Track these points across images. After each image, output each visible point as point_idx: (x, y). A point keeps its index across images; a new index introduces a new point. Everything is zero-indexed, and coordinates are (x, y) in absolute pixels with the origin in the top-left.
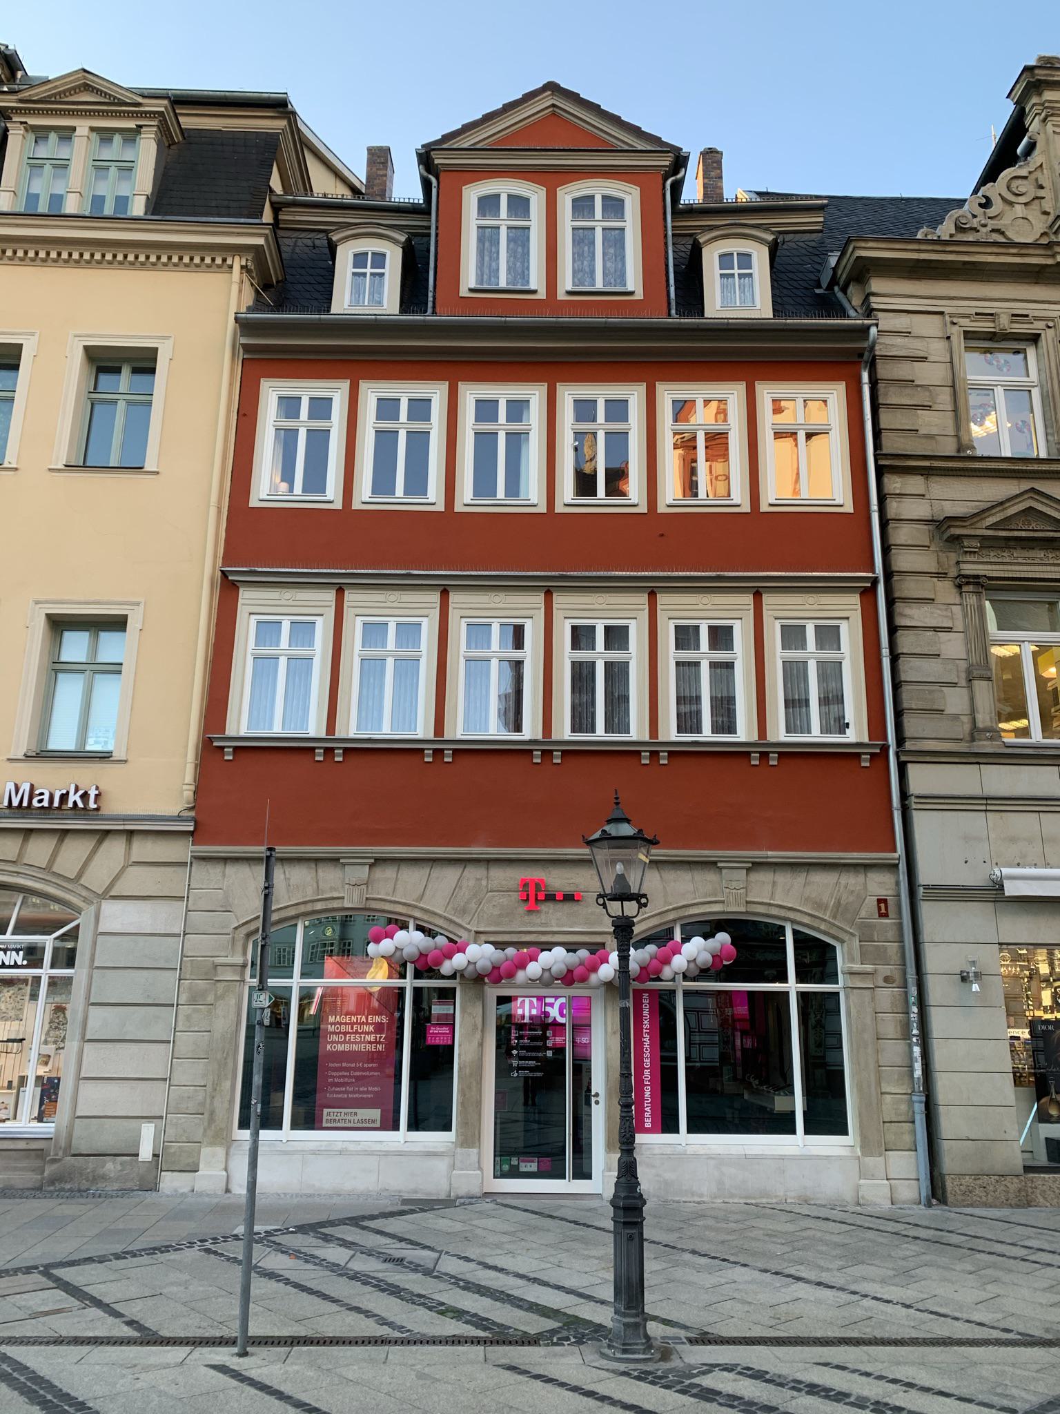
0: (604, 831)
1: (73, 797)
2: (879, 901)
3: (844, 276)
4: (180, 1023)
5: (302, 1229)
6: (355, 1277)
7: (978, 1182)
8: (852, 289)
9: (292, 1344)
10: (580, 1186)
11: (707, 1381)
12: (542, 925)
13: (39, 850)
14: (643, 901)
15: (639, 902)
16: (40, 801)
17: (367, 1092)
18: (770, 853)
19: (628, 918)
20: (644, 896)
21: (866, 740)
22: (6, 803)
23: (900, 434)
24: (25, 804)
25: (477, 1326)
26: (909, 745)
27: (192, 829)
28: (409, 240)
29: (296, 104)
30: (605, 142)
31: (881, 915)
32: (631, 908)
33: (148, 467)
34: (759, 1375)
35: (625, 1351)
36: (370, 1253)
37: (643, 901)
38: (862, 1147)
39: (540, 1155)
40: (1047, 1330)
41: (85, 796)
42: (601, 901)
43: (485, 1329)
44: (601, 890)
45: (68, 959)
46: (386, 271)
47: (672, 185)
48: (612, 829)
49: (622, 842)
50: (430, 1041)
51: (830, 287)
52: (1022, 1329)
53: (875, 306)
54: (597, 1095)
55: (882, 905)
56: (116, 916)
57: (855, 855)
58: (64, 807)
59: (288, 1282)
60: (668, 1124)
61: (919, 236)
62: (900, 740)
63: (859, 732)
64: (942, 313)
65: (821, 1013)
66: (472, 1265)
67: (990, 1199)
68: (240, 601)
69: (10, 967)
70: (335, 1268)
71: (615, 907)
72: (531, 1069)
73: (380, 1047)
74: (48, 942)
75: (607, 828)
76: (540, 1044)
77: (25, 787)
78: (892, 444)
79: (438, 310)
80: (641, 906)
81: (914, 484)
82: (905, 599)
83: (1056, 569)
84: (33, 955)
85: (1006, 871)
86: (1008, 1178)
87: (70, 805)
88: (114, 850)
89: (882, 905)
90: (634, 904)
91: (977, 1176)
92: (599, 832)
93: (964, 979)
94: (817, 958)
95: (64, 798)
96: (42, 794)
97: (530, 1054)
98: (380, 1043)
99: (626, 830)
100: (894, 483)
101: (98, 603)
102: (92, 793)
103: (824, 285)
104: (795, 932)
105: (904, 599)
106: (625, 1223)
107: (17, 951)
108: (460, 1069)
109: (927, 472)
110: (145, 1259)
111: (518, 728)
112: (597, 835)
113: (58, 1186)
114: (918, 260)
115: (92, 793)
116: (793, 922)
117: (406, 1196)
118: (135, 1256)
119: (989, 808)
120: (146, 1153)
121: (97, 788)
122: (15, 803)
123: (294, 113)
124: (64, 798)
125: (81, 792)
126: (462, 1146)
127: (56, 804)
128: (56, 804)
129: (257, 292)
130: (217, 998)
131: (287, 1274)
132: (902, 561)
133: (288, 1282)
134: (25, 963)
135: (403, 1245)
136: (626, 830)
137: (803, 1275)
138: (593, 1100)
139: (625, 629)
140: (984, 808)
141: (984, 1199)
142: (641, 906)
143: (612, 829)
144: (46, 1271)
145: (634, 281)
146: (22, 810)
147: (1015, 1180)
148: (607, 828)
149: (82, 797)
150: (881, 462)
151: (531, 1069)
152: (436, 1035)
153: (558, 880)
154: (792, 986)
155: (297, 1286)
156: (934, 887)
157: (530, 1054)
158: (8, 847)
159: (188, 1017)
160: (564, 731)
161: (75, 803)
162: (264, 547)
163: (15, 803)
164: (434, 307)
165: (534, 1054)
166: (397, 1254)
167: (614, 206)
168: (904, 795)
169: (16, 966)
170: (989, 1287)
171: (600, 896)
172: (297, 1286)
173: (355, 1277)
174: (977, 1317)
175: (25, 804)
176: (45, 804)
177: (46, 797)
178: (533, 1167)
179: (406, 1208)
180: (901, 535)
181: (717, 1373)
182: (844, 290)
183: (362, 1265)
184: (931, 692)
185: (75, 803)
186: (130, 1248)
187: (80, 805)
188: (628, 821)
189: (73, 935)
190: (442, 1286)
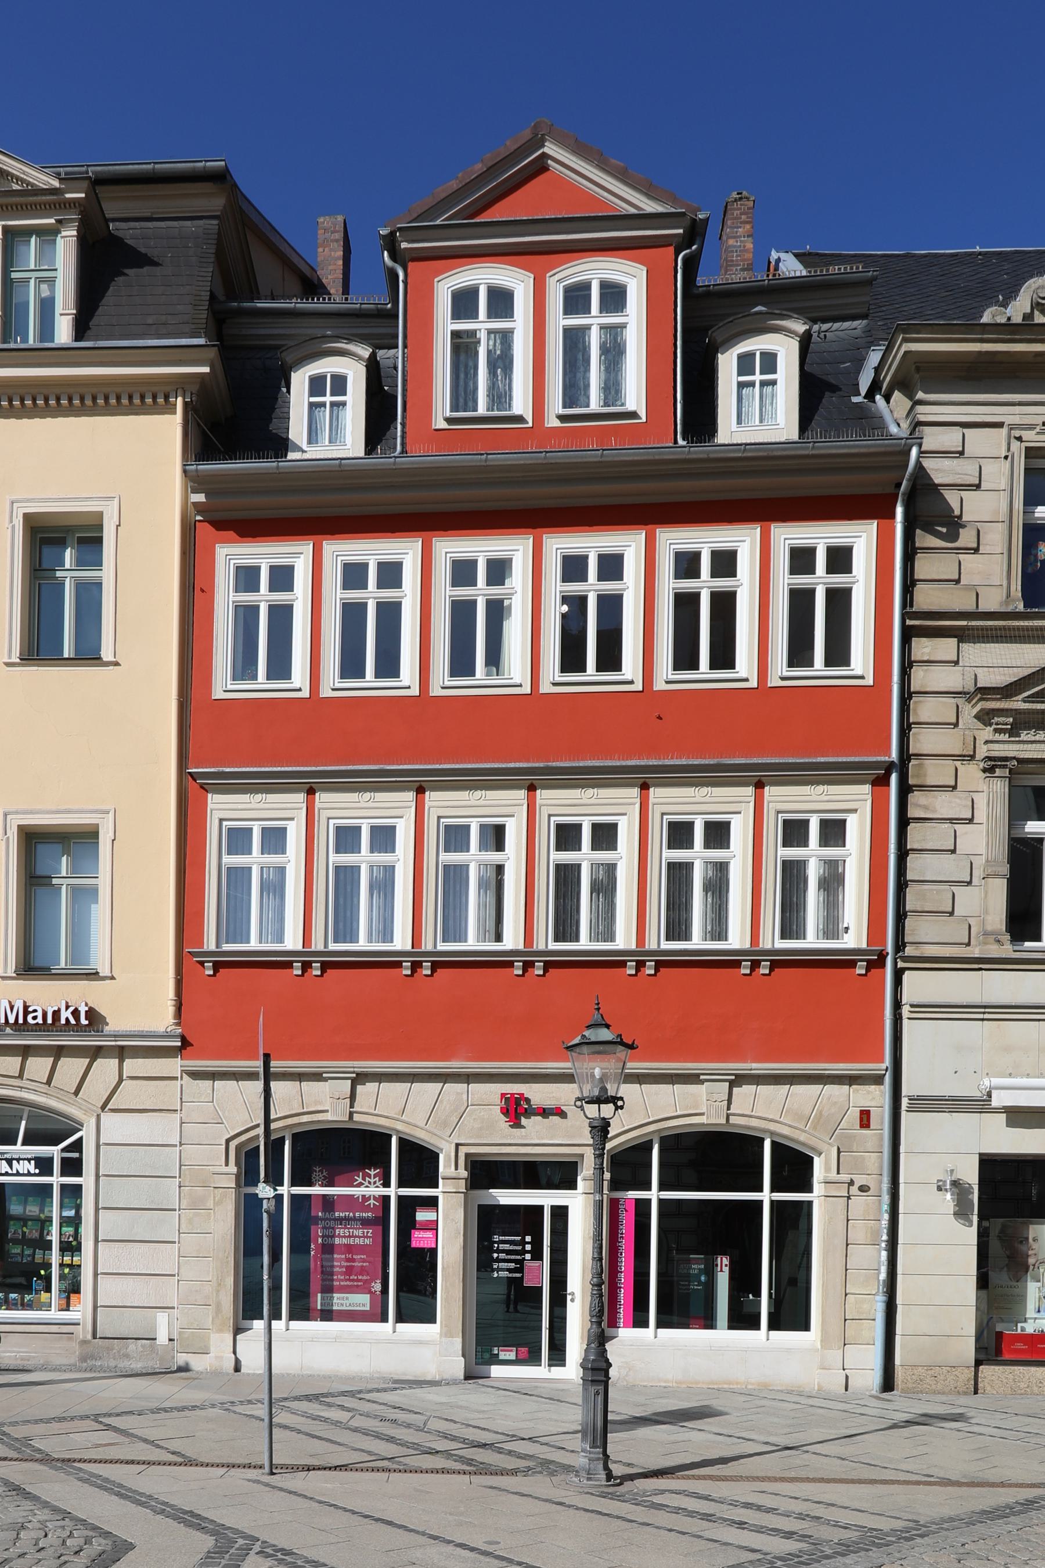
0: (584, 1036)
1: (65, 1015)
2: (862, 1112)
3: (888, 378)
4: (183, 1226)
5: (308, 1398)
6: (356, 1430)
7: (929, 1372)
8: (897, 395)
9: (309, 1470)
10: (557, 1372)
11: (657, 1499)
12: (522, 1137)
13: (38, 1066)
14: (620, 1103)
15: (615, 1104)
16: (35, 1018)
17: (358, 1280)
18: (754, 1065)
19: (604, 1119)
20: (621, 1099)
21: (864, 946)
22: (3, 1021)
23: (936, 586)
24: (21, 1021)
25: (463, 1463)
26: (909, 951)
27: (179, 1044)
28: (373, 355)
29: (240, 178)
30: (604, 204)
31: (862, 1126)
32: (607, 1110)
33: (107, 655)
34: (706, 1498)
35: (589, 1479)
36: (367, 1415)
37: (620, 1103)
38: (822, 1341)
39: (517, 1345)
40: (964, 1476)
41: (76, 1013)
42: (579, 1103)
43: (471, 1465)
44: (579, 1435)
45: (73, 1167)
46: (348, 398)
47: (685, 261)
48: (591, 1035)
49: (601, 1048)
50: (414, 1244)
51: (870, 395)
52: (941, 1475)
53: (922, 418)
54: (573, 1294)
55: (865, 1122)
56: (115, 1127)
57: (842, 1066)
58: (57, 1024)
59: (299, 1432)
60: (640, 1322)
61: (986, 318)
62: (900, 945)
63: (859, 938)
64: (999, 425)
65: (793, 1222)
66: (458, 1426)
67: (939, 1387)
68: (210, 806)
69: (23, 1175)
70: (337, 1423)
71: (592, 1110)
72: (510, 1270)
73: (367, 1241)
74: (55, 1151)
75: (587, 1033)
76: (520, 1248)
77: (19, 1005)
78: (926, 598)
79: (408, 448)
80: (617, 1108)
81: (946, 647)
82: (921, 787)
83: (1042, 746)
84: (44, 1165)
85: (996, 1081)
86: (960, 1369)
87: (63, 1022)
88: (106, 1068)
89: (865, 1117)
90: (611, 1106)
91: (930, 1367)
92: (579, 1037)
93: (939, 1189)
94: (794, 1168)
95: (56, 1014)
96: (35, 1011)
97: (509, 1257)
98: (367, 1237)
99: (605, 1034)
100: (922, 648)
101: (69, 812)
102: (83, 1009)
103: (863, 390)
104: (773, 1143)
105: (921, 787)
106: (592, 1381)
107: (29, 1160)
108: (443, 1268)
109: (962, 636)
110: (175, 1414)
111: (499, 938)
112: (577, 1041)
113: (90, 1363)
114: (980, 352)
115: (83, 1009)
116: (772, 1133)
117: (396, 1377)
118: (166, 1411)
119: (986, 1016)
120: (162, 1338)
121: (86, 1005)
122: (12, 1020)
123: (235, 185)
124: (56, 1014)
125: (71, 1009)
126: (446, 1336)
127: (50, 1021)
128: (50, 1021)
129: (204, 433)
130: (216, 1204)
131: (298, 1427)
132: (922, 741)
133: (299, 1432)
134: (37, 1171)
135: (397, 1410)
136: (605, 1034)
137: (752, 1437)
138: (569, 1297)
139: (614, 827)
140: (981, 1016)
141: (934, 1387)
142: (617, 1108)
143: (591, 1035)
144: (96, 1418)
145: (634, 396)
146: (21, 1027)
147: (966, 1371)
148: (587, 1033)
149: (73, 1013)
150: (908, 622)
151: (510, 1270)
152: (420, 1239)
153: (538, 1094)
154: (766, 1196)
155: (307, 1434)
156: (920, 1098)
157: (509, 1257)
158: (11, 1064)
159: (190, 1221)
160: (545, 941)
161: (67, 1019)
162: (222, 746)
163: (12, 1020)
164: (403, 444)
165: (513, 1257)
166: (393, 1417)
167: (614, 296)
168: (897, 1005)
169: (29, 1174)
170: (919, 1448)
171: (578, 1099)
172: (307, 1434)
173: (356, 1430)
174: (904, 1467)
175: (21, 1021)
176: (40, 1020)
177: (39, 1014)
178: (511, 1355)
179: (397, 1386)
180: (924, 710)
181: (667, 1494)
182: (887, 398)
183: (358, 1422)
184: (938, 891)
185: (67, 1019)
186: (162, 1406)
187: (73, 1021)
188: (608, 1026)
189: (78, 1146)
190: (432, 1438)
